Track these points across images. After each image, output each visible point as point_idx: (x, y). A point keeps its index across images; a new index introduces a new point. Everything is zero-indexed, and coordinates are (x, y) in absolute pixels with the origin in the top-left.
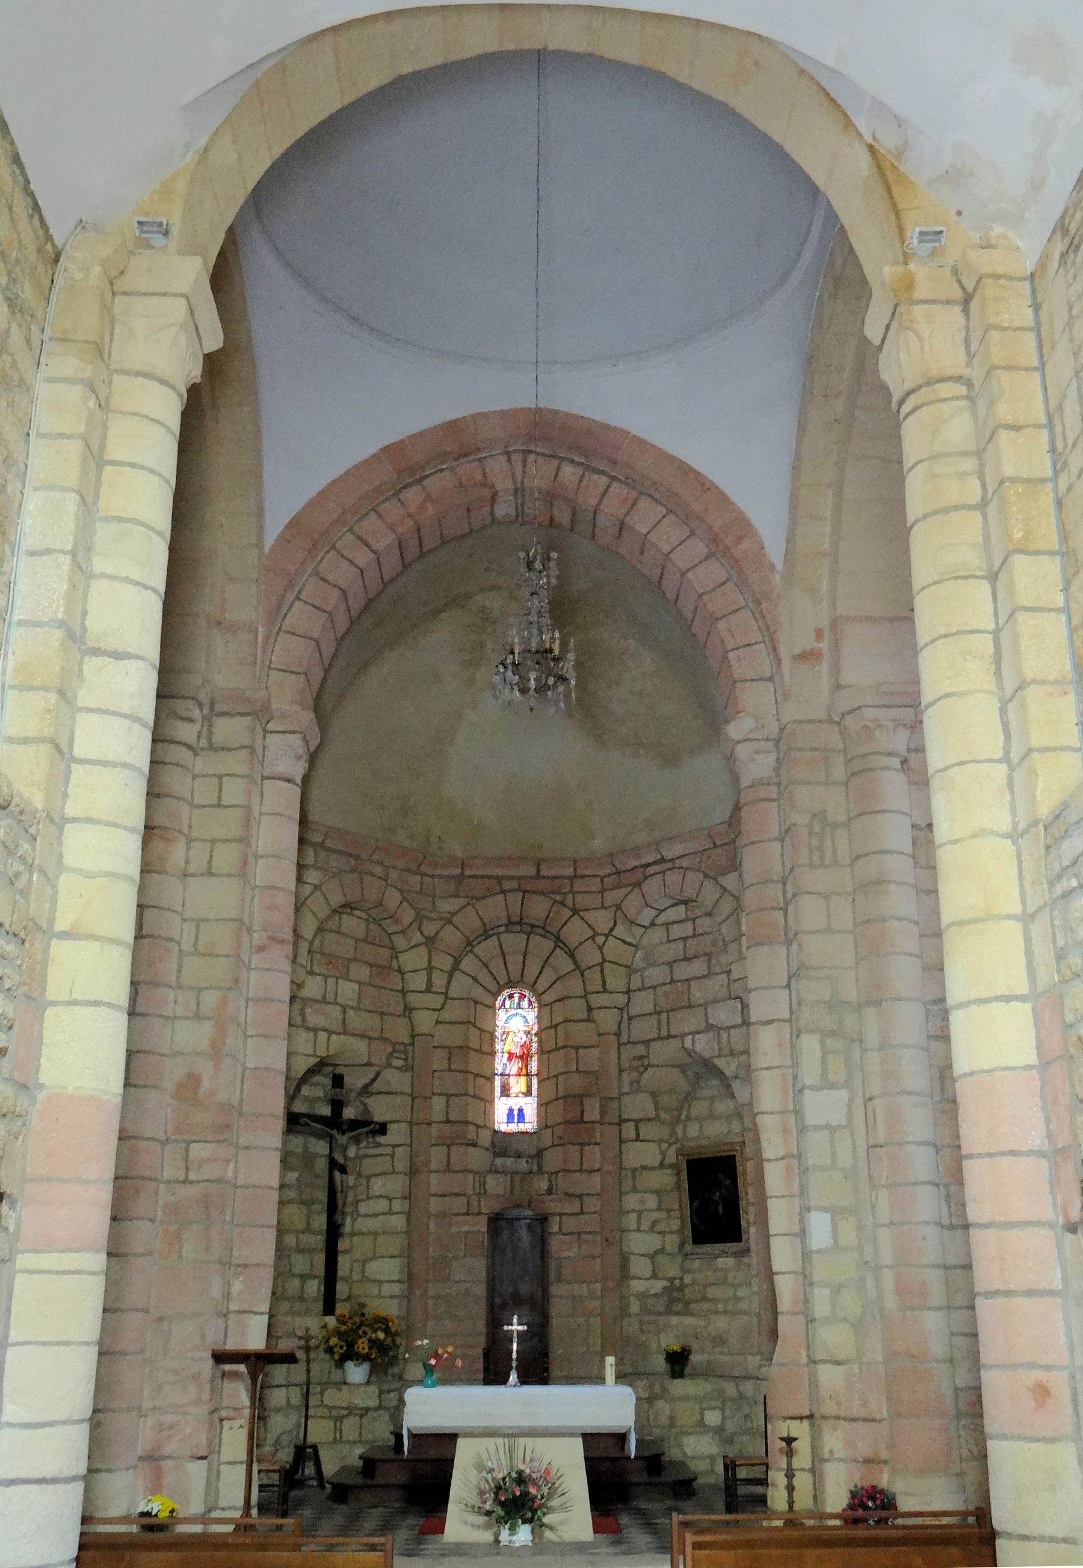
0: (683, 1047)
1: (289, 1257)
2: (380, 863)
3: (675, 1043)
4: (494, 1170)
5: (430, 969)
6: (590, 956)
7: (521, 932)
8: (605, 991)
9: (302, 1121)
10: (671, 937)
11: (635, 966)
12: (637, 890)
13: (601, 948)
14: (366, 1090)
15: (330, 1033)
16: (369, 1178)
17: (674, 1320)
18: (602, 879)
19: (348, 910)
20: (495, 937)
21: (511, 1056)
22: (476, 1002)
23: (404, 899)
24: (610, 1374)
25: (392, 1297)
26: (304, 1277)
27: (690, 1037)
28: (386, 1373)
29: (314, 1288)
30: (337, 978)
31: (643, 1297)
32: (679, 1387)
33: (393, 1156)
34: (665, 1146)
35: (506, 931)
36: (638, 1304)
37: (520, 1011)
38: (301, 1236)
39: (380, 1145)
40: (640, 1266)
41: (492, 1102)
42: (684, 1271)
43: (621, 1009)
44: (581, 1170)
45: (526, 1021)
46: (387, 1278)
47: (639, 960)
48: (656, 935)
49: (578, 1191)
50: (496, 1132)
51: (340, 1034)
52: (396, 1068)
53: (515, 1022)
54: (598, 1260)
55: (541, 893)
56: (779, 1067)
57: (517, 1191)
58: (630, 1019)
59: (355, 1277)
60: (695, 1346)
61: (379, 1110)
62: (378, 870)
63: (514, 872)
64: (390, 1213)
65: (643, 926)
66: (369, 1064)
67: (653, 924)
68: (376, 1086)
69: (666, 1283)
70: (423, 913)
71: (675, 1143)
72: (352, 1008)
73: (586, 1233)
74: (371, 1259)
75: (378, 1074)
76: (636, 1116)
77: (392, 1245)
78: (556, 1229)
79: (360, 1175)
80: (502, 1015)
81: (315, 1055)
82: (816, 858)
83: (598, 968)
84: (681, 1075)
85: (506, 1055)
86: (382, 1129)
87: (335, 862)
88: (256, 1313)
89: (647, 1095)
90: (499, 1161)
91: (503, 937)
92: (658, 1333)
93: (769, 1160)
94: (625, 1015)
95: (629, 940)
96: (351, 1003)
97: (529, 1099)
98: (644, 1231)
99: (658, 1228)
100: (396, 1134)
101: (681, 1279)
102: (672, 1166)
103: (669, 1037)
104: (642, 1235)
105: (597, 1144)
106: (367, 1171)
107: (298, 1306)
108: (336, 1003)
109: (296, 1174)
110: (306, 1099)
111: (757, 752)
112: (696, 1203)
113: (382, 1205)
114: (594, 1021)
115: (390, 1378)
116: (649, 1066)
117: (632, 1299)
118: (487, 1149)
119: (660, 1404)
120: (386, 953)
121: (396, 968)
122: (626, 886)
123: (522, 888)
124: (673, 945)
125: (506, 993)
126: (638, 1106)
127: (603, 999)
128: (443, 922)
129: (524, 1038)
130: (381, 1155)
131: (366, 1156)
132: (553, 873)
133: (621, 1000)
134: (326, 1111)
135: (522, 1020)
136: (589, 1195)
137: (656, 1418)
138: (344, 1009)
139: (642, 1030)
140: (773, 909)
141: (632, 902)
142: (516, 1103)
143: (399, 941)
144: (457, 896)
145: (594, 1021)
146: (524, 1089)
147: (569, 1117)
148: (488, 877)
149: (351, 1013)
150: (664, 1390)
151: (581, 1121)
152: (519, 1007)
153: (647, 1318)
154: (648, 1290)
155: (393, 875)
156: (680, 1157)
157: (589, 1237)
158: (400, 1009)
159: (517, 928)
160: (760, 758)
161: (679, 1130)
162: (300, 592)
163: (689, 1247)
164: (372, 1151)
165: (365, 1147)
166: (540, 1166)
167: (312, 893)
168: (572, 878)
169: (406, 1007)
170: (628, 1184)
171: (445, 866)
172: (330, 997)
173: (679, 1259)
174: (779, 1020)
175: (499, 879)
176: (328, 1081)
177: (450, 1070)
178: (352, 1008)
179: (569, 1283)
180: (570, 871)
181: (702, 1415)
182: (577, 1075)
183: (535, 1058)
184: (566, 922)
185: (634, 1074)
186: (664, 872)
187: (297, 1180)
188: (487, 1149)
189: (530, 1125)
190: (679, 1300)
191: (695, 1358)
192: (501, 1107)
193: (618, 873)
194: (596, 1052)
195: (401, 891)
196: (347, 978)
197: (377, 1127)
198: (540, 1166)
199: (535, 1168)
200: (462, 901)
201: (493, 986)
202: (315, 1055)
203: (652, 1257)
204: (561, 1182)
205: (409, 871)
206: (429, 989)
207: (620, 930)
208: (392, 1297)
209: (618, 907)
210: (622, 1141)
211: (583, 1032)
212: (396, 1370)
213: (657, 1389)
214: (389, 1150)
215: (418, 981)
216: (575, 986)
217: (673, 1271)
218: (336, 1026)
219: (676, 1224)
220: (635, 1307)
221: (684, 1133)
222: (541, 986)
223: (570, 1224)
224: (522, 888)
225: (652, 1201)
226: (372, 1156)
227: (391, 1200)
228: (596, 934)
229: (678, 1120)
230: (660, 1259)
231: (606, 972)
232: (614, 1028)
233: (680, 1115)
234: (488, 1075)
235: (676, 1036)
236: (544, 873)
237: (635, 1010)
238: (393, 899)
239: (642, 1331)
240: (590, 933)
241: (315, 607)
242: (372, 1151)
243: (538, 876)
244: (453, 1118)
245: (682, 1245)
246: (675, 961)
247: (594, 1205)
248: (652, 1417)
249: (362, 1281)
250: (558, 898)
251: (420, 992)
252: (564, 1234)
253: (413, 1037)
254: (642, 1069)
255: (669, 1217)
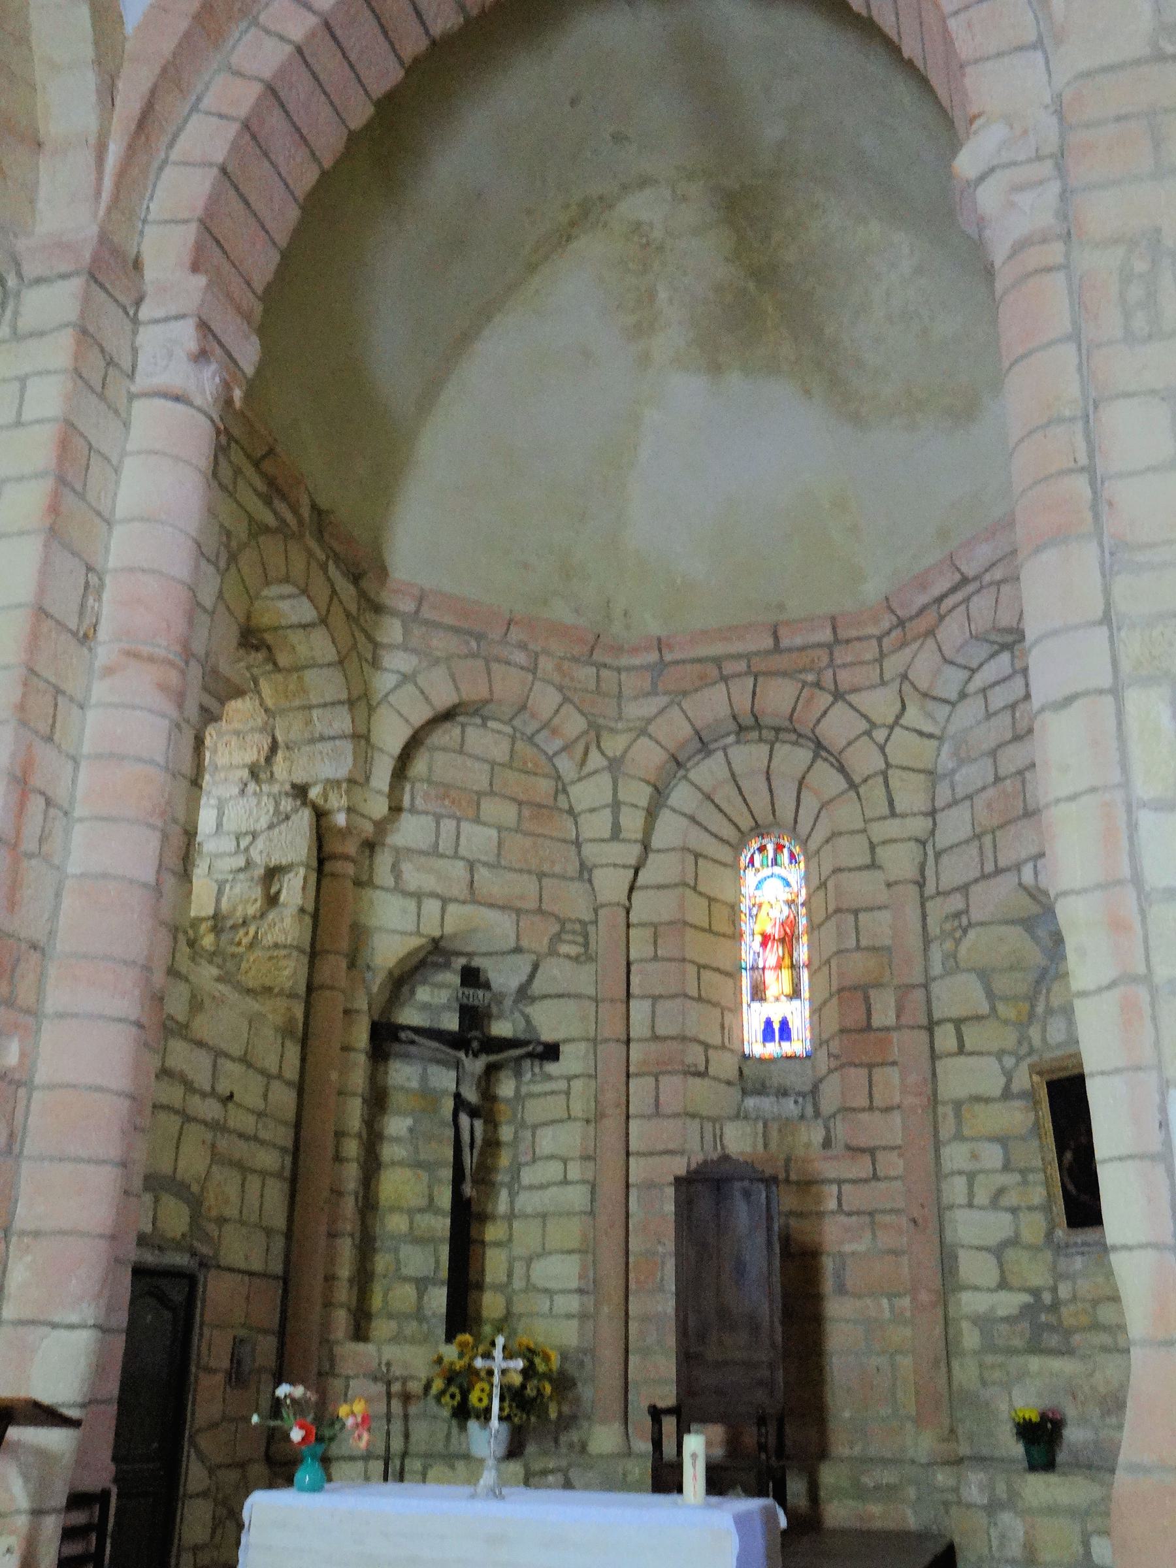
0: (1020, 884)
1: (396, 1250)
2: (522, 646)
3: (1007, 882)
4: (740, 1115)
5: (616, 805)
6: (863, 760)
7: (761, 740)
8: (893, 814)
9: (403, 1035)
10: (992, 709)
11: (940, 770)
12: (930, 642)
13: (882, 748)
14: (524, 993)
15: (445, 901)
16: (535, 1127)
17: (1035, 1363)
18: (880, 639)
19: (479, 721)
20: (720, 754)
21: (766, 939)
22: (697, 856)
23: (566, 700)
24: (694, 1476)
25: (569, 1316)
26: (422, 1284)
27: (1030, 865)
28: (556, 1441)
29: (438, 1299)
30: (459, 820)
31: (983, 1322)
32: (1039, 1488)
33: (568, 1093)
34: (1009, 1062)
35: (738, 742)
36: (977, 1332)
37: (776, 870)
38: (418, 1217)
39: (549, 1078)
40: (975, 1268)
41: (737, 1009)
42: (1059, 1276)
43: (923, 843)
44: (871, 1108)
45: (788, 884)
46: (560, 1286)
47: (946, 761)
48: (971, 710)
49: (862, 1141)
50: (746, 1058)
51: (464, 902)
52: (568, 957)
53: (771, 889)
54: (905, 1260)
55: (785, 674)
56: (1093, 790)
57: (773, 1145)
58: (938, 855)
59: (518, 1284)
60: (1071, 1412)
61: (549, 1022)
62: (520, 657)
63: (737, 647)
64: (565, 1182)
65: (945, 701)
66: (518, 950)
67: (963, 695)
68: (537, 987)
69: (1026, 1298)
70: (601, 721)
71: (1029, 1054)
72: (485, 864)
73: (884, 1212)
74: (539, 1256)
75: (536, 967)
76: (956, 1012)
77: (568, 1232)
78: (832, 1205)
79: (523, 1125)
80: (750, 879)
81: (418, 933)
82: (1140, 322)
83: (880, 779)
84: (1026, 935)
85: (758, 939)
86: (551, 1052)
87: (441, 643)
88: (54, 1326)
89: (973, 977)
90: (750, 1102)
91: (731, 752)
92: (1007, 1386)
93: (1083, 994)
94: (930, 852)
95: (928, 728)
96: (484, 858)
97: (796, 1003)
98: (981, 1208)
99: (1005, 1201)
100: (572, 1060)
101: (1054, 1290)
102: (1023, 1095)
103: (998, 871)
104: (976, 1215)
105: (894, 1063)
106: (530, 1119)
107: (411, 1328)
108: (456, 856)
109: (409, 1122)
110: (426, 1007)
111: (1019, 188)
112: (1069, 1156)
113: (553, 1170)
114: (880, 867)
115: (564, 1450)
116: (970, 925)
117: (965, 1325)
118: (729, 1083)
119: (1006, 1518)
120: (544, 787)
121: (567, 807)
122: (915, 639)
123: (754, 669)
124: (994, 721)
125: (755, 845)
126: (958, 995)
127: (892, 828)
128: (633, 735)
129: (786, 910)
130: (553, 1093)
131: (531, 1095)
132: (798, 641)
133: (919, 826)
134: (451, 1022)
135: (779, 883)
136: (884, 1148)
137: (1002, 1545)
138: (471, 866)
139: (957, 869)
140: (1062, 473)
141: (923, 663)
142: (776, 1009)
143: (566, 765)
144: (654, 692)
145: (880, 867)
146: (788, 989)
147: (849, 1023)
148: (699, 660)
149: (482, 873)
150: (1014, 1495)
151: (869, 1027)
152: (775, 862)
153: (989, 1359)
154: (993, 1308)
155: (546, 665)
156: (1036, 1078)
157: (887, 1219)
158: (572, 868)
159: (754, 735)
160: (1025, 199)
161: (1034, 1033)
162: (199, 99)
163: (1061, 1233)
164: (537, 1088)
165: (532, 1081)
166: (816, 1106)
167: (398, 686)
168: (829, 647)
169: (582, 864)
170: (947, 1128)
171: (635, 650)
172: (445, 845)
173: (1048, 1255)
174: (1086, 693)
175: (718, 661)
176: (452, 978)
177: (656, 958)
178: (485, 864)
179: (859, 1296)
180: (826, 635)
181: (1086, 1544)
182: (858, 956)
183: (804, 939)
184: (825, 713)
185: (949, 945)
186: (967, 600)
187: (411, 1130)
188: (729, 1083)
189: (797, 1046)
190: (1051, 1328)
191: (1073, 1435)
192: (753, 1017)
193: (901, 623)
194: (885, 916)
195: (560, 689)
196: (477, 820)
197: (540, 1049)
198: (816, 1106)
199: (809, 1111)
200: (662, 700)
201: (728, 832)
202: (418, 933)
203: (998, 1251)
204: (840, 1130)
205: (575, 659)
206: (616, 833)
207: (913, 716)
208: (569, 1316)
209: (905, 677)
210: (934, 1056)
211: (865, 887)
212: (574, 1436)
213: (1001, 1489)
214: (562, 1085)
215: (597, 825)
216: (847, 814)
217: (1035, 1272)
218: (458, 889)
219: (1038, 1195)
220: (970, 1338)
221: (1044, 1039)
222: (804, 827)
223: (854, 1197)
224: (754, 669)
225: (992, 1155)
226: (539, 1095)
227: (565, 1161)
228: (873, 725)
229: (1031, 1015)
230: (1011, 1254)
231: (894, 783)
232: (911, 872)
233: (1033, 1006)
234: (728, 967)
235: (1008, 869)
236: (785, 643)
237: (943, 839)
238: (546, 700)
239: (984, 1383)
240: (864, 725)
241: (221, 116)
242: (537, 1088)
243: (777, 648)
244: (661, 1031)
245: (1049, 1234)
246: (999, 746)
247: (892, 1164)
248: (995, 1543)
249: (526, 1291)
250: (810, 678)
251: (603, 840)
252: (849, 1214)
253: (596, 911)
254: (958, 934)
255: (1025, 1182)
